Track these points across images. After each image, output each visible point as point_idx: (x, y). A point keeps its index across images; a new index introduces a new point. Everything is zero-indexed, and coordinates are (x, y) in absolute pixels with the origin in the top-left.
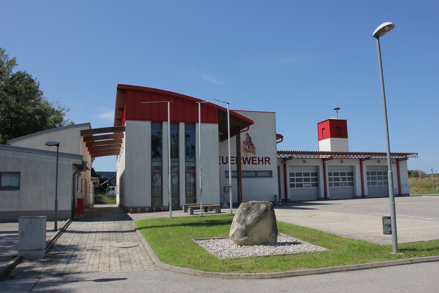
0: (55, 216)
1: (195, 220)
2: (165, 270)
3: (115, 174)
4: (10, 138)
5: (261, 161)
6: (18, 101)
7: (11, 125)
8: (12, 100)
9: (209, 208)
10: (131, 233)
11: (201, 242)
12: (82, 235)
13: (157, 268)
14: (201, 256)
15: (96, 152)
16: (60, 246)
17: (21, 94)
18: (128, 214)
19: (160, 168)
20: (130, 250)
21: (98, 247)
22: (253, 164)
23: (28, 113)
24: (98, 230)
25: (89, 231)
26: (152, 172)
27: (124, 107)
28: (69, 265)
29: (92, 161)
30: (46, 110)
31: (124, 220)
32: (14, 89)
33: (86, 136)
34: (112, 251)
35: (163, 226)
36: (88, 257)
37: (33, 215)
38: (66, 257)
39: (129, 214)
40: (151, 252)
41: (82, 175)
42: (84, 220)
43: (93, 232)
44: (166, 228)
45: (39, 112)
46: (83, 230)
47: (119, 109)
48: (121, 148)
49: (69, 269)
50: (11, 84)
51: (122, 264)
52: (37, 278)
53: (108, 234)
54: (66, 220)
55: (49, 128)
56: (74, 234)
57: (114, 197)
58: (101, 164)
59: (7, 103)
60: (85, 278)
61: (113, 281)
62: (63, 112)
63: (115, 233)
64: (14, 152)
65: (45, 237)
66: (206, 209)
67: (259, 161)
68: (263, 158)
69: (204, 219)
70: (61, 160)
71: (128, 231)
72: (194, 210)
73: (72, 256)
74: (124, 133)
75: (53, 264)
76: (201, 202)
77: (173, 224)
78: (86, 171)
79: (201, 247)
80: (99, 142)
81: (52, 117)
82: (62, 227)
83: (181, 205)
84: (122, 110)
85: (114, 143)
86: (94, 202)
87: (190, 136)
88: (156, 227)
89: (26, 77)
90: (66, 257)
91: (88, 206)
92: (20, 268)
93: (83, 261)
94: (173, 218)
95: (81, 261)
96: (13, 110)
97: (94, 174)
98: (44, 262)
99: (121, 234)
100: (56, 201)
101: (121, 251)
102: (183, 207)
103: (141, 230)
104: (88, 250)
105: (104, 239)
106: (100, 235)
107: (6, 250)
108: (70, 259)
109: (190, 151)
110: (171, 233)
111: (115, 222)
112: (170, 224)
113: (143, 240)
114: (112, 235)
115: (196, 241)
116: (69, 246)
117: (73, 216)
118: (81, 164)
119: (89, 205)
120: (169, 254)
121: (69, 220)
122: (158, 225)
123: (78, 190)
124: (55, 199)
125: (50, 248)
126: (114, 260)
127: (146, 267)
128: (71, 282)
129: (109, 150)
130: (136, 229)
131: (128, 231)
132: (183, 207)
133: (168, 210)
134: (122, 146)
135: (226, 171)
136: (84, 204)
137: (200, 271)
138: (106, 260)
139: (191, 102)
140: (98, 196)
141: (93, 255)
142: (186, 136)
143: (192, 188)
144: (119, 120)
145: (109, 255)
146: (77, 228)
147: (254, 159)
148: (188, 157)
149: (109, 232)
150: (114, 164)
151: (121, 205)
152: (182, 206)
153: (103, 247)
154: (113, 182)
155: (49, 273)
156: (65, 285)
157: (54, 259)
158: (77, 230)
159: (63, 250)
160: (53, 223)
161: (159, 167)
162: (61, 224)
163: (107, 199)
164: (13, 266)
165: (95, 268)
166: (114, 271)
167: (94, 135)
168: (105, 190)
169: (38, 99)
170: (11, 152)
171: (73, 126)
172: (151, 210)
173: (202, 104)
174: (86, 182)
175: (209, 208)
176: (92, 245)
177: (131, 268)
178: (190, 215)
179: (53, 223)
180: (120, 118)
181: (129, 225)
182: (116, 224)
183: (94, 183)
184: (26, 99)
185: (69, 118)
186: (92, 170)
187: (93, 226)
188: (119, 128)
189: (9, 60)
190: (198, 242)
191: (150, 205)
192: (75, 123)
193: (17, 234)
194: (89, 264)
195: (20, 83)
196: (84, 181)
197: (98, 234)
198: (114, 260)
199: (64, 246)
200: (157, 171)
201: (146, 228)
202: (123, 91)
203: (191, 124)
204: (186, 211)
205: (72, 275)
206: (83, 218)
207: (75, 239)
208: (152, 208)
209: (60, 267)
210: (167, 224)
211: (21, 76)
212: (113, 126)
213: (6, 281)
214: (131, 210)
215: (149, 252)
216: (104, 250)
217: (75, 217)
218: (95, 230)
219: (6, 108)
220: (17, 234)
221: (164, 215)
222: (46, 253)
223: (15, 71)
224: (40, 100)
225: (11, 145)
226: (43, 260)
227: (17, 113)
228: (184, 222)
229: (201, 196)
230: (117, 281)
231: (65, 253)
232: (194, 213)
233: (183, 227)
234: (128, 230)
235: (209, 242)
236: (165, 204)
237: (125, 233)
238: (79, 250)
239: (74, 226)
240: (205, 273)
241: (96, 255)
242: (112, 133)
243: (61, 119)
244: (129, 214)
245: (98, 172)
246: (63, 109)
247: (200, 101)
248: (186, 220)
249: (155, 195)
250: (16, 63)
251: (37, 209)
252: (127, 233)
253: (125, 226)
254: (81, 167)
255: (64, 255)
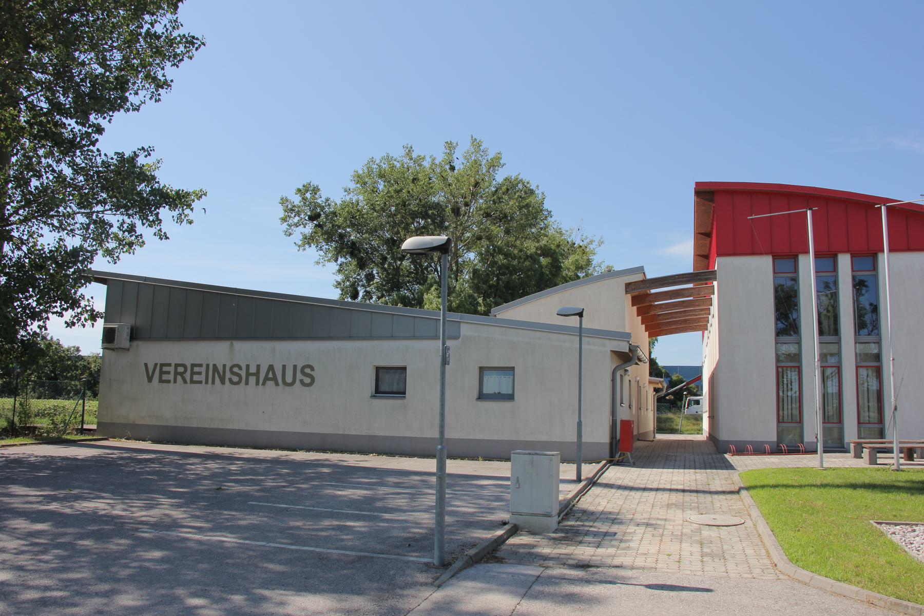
0: (576, 454)
1: (879, 477)
2: (799, 582)
3: (699, 369)
4: (497, 304)
5: (252, 374)
6: (507, 232)
7: (498, 279)
8: (498, 230)
9: (919, 451)
10: (729, 496)
11: (893, 529)
12: (632, 494)
13: (781, 577)
14: (890, 563)
15: (657, 325)
16: (584, 512)
17: (512, 218)
18: (726, 456)
19: (796, 358)
20: (724, 531)
21: (658, 519)
22: (161, 381)
23: (526, 253)
24: (661, 486)
25: (643, 486)
26: (777, 367)
27: (712, 228)
28: (601, 551)
29: (651, 344)
30: (558, 246)
31: (716, 468)
32: (500, 212)
33: (636, 293)
34: (687, 531)
35: (801, 486)
36: (637, 537)
37: (535, 448)
38: (595, 534)
39: (727, 456)
40: (769, 540)
41: (629, 373)
42: (634, 465)
43: (651, 489)
44: (807, 491)
45: (546, 252)
46: (631, 484)
47: (703, 234)
48: (710, 317)
49: (599, 558)
50: (494, 202)
51: (705, 559)
52: (541, 566)
53: (680, 495)
54: (598, 463)
55: (566, 280)
56: (613, 491)
57: (698, 418)
58: (672, 350)
59: (489, 238)
60: (630, 578)
61: (684, 593)
62: (592, 247)
63: (695, 494)
64: (503, 329)
65: (558, 492)
66: (909, 454)
67: (248, 374)
68: (258, 367)
69: (903, 477)
70: (589, 344)
71: (723, 492)
72: (879, 455)
73: (606, 534)
74: (715, 283)
75: (571, 545)
76: (894, 438)
77: (825, 482)
78: (637, 364)
79: (892, 542)
80: (661, 305)
81: (572, 259)
82: (591, 475)
83: (846, 440)
84: (708, 235)
85: (694, 306)
86: (657, 427)
87: (863, 285)
88: (786, 486)
89: (520, 186)
90: (595, 534)
91: (642, 437)
92: (514, 545)
93: (627, 544)
94: (826, 469)
95: (623, 545)
96: (500, 251)
97: (655, 370)
98: (554, 539)
99: (708, 497)
100: (580, 424)
101: (706, 533)
102: (852, 445)
103: (752, 492)
104: (638, 525)
105: (672, 504)
106: (665, 496)
107: (492, 510)
108: (603, 538)
109: (868, 318)
110: (819, 503)
111: (698, 471)
112: (819, 483)
113: (755, 513)
114: (688, 497)
115: (878, 526)
116: (602, 513)
117: (612, 455)
118: (627, 350)
119: (645, 434)
120: (810, 548)
121: (604, 462)
122: (790, 483)
123: (622, 403)
124: (577, 420)
125: (566, 514)
126: (690, 549)
127: (756, 571)
128: (601, 582)
129: (685, 321)
130: (741, 489)
131: (723, 492)
132: (852, 445)
133: (815, 452)
134: (712, 313)
135: (378, 392)
136: (635, 433)
137: (884, 597)
138: (674, 547)
139: (865, 206)
140: (664, 416)
141: (648, 536)
142: (854, 286)
143: (873, 404)
144: (703, 256)
145: (681, 538)
146: (620, 479)
147: (165, 369)
148: (865, 331)
149: (684, 491)
150: (694, 350)
151: (712, 437)
152: (849, 444)
153: (670, 520)
154: (697, 387)
155: (562, 561)
156: (591, 587)
157: (572, 536)
158: (619, 483)
159: (591, 521)
160: (575, 466)
161: (795, 354)
162: (589, 470)
163: (685, 422)
164: (501, 541)
165: (650, 562)
166: (689, 572)
167: (653, 291)
168: (679, 403)
169: (543, 225)
170: (497, 329)
171: (610, 273)
172: (777, 450)
173: (890, 210)
174: (639, 387)
175: (919, 451)
176: (646, 516)
177: (723, 569)
178: (868, 466)
179: (575, 466)
180: (706, 253)
181: (726, 479)
182: (698, 476)
183: (656, 390)
184: (523, 228)
185: (605, 258)
186: (652, 362)
187: (652, 478)
188: (702, 275)
189: (489, 158)
190: (884, 528)
191: (775, 440)
192: (617, 268)
193: (509, 483)
194: (639, 551)
195: (510, 198)
196: (634, 384)
197: (659, 494)
198: (690, 549)
199: (592, 513)
200: (788, 366)
201: (763, 487)
202: (707, 194)
203: (867, 255)
204: (858, 455)
205: (605, 570)
206: (631, 461)
207: (614, 501)
208: (778, 446)
209: (584, 552)
210: (810, 481)
211: (511, 186)
212: (692, 271)
213: (490, 565)
214: (732, 447)
215: (765, 540)
216: (670, 527)
217: (617, 457)
218: (655, 486)
219: (488, 247)
220: (509, 483)
221: (805, 461)
222: (559, 522)
223: (500, 176)
224: (546, 227)
225: (498, 317)
226: (554, 535)
227: (507, 255)
228: (853, 482)
229: (895, 423)
230: (693, 593)
231: (595, 527)
232: (879, 461)
233: (849, 491)
234: (724, 489)
235: (914, 531)
236: (808, 437)
237: (716, 496)
238: (621, 523)
239: (614, 474)
240: (899, 604)
241: (653, 535)
242: (691, 286)
243: (589, 263)
244: (727, 456)
245: (664, 367)
246: (591, 242)
247: (885, 201)
248: (857, 475)
249: (786, 417)
250: (502, 162)
251: (544, 438)
252: (722, 497)
253: (717, 482)
254: (626, 358)
255: (592, 529)
